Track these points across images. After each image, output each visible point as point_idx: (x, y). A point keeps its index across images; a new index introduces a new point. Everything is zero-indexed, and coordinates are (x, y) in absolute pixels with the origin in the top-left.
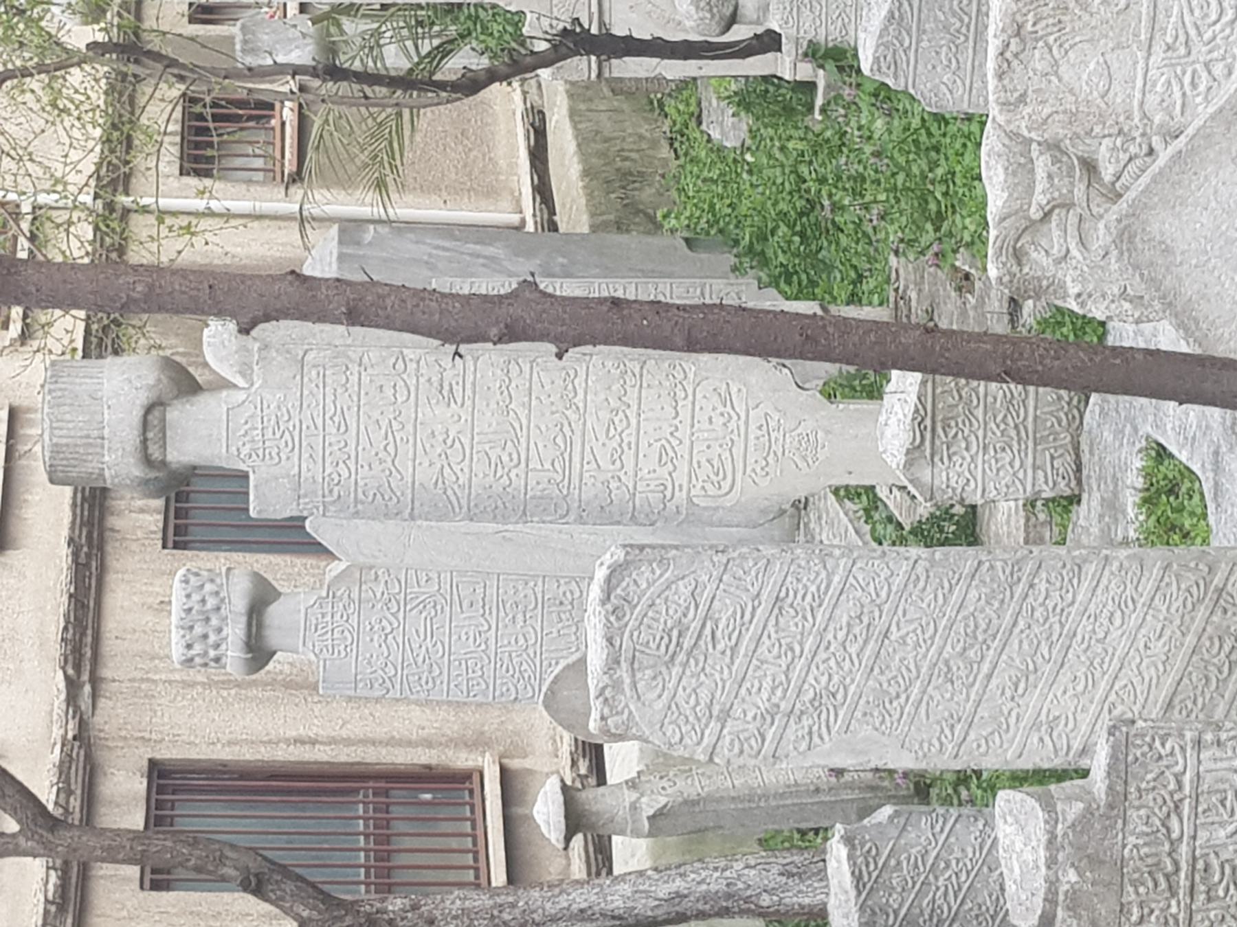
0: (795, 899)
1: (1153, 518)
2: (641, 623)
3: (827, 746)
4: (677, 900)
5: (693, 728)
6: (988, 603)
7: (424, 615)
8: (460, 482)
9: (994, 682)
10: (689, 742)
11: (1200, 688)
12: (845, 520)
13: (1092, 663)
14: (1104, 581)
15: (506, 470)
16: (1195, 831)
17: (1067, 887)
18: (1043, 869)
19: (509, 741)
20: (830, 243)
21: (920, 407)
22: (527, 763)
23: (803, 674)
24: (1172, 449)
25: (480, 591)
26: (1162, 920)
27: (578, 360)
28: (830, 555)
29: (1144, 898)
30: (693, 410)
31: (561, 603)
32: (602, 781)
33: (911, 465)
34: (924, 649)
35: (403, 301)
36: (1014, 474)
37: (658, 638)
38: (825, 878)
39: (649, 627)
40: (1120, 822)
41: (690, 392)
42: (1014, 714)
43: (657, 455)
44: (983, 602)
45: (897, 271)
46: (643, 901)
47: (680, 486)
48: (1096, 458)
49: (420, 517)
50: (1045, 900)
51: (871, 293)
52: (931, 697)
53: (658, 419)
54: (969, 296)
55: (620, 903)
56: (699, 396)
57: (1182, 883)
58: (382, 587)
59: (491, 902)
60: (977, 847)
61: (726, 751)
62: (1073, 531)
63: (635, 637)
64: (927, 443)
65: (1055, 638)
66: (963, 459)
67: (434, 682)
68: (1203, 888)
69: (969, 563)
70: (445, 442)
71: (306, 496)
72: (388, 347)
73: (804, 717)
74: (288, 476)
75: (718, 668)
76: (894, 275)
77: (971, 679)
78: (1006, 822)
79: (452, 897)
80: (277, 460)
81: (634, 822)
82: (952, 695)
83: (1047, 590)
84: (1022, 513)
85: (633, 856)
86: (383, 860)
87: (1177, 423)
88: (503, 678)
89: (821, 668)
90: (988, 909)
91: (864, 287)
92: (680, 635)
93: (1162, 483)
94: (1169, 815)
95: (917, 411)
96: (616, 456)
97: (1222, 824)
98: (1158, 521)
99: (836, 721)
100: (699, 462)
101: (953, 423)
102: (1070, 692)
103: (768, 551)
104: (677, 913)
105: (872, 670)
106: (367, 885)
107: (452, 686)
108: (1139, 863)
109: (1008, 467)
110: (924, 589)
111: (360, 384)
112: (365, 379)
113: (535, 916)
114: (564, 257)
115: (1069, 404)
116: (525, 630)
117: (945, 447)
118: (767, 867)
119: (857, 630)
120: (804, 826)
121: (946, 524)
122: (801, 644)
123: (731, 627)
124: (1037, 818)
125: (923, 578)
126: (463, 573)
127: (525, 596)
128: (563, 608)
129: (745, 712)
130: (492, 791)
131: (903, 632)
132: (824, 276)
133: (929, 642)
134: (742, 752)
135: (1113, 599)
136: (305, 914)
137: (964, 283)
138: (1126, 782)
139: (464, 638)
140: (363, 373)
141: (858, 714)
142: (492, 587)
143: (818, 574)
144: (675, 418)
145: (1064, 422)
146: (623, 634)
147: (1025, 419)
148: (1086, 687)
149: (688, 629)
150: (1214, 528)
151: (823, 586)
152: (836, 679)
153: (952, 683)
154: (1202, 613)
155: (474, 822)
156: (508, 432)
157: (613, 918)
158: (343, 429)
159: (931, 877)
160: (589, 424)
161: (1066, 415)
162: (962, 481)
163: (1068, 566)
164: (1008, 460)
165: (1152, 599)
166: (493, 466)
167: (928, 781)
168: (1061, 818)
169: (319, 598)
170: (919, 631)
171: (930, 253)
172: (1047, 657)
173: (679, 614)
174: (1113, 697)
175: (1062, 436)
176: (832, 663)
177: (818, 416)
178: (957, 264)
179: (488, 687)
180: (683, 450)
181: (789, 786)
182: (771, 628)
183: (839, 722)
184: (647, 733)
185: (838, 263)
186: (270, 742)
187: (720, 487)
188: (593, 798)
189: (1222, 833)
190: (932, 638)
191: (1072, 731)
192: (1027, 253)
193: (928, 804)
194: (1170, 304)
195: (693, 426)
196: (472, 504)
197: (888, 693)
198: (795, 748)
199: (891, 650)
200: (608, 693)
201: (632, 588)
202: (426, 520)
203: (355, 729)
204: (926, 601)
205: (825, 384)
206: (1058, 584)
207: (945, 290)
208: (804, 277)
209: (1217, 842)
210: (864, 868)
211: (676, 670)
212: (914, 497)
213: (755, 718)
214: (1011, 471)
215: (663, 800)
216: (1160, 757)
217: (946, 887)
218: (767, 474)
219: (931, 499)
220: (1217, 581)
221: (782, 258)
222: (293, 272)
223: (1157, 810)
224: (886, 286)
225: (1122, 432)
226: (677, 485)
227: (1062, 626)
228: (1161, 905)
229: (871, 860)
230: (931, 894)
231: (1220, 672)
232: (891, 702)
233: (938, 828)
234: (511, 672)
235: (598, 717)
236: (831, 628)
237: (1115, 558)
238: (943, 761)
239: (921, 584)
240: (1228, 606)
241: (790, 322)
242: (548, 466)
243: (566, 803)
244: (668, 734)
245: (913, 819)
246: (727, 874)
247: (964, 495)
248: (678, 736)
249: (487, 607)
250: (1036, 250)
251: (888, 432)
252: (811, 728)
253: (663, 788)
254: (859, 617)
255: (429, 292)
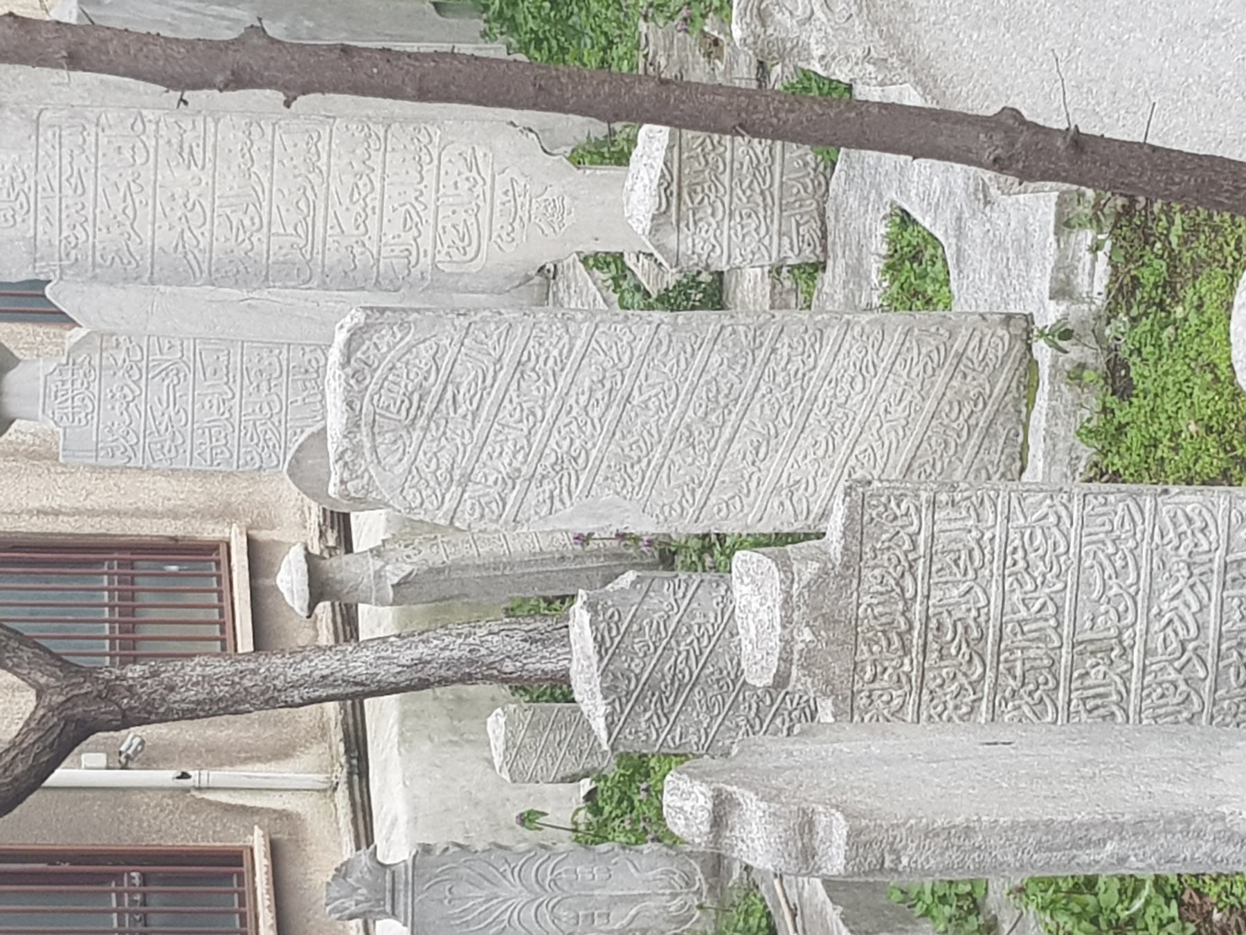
0: (538, 665)
1: (897, 284)
2: (381, 387)
3: (568, 510)
4: (420, 667)
5: (434, 493)
6: (729, 367)
7: (166, 382)
8: (201, 246)
9: (736, 446)
10: (431, 507)
11: (939, 453)
12: (594, 289)
13: (832, 428)
14: (846, 346)
15: (248, 234)
16: (929, 590)
17: (803, 645)
18: (779, 629)
19: (256, 512)
20: (581, 9)
21: (666, 172)
22: (274, 535)
23: (545, 439)
24: (916, 215)
25: (223, 358)
26: (895, 678)
27: (321, 122)
28: (572, 319)
29: (878, 656)
30: (439, 174)
31: (307, 371)
32: (349, 550)
33: (657, 231)
34: (666, 414)
35: (126, 45)
36: (760, 241)
37: (398, 403)
38: (568, 644)
39: (390, 390)
40: (855, 582)
41: (435, 156)
42: (755, 478)
43: (402, 220)
44: (725, 366)
45: (646, 36)
46: (386, 667)
47: (425, 251)
48: (842, 224)
49: (160, 281)
50: (779, 659)
51: (620, 59)
52: (673, 462)
53: (402, 183)
54: (717, 61)
55: (362, 670)
56: (444, 159)
57: (915, 642)
58: (123, 355)
59: (232, 669)
60: (719, 613)
61: (467, 516)
62: (818, 298)
63: (375, 402)
64: (673, 209)
65: (796, 402)
66: (710, 225)
67: (177, 451)
68: (935, 646)
69: (712, 327)
70: (185, 205)
71: (42, 258)
72: (126, 108)
73: (545, 482)
74: (24, 238)
75: (459, 432)
76: (643, 41)
77: (712, 444)
78: (742, 582)
79: (192, 664)
80: (12, 222)
81: (378, 591)
82: (694, 460)
83: (789, 354)
84: (768, 281)
85: (379, 625)
86: (127, 632)
87: (921, 189)
88: (247, 446)
89: (563, 433)
90: (729, 673)
91: (614, 54)
92: (421, 399)
93: (906, 249)
94: (903, 575)
95: (663, 176)
96: (360, 221)
97: (956, 584)
98: (902, 288)
99: (577, 485)
100: (444, 228)
101: (699, 189)
102: (811, 457)
103: (510, 315)
104: (420, 679)
105: (614, 434)
106: (112, 656)
107: (195, 454)
108: (873, 622)
109: (754, 234)
110: (666, 353)
111: (97, 145)
112: (103, 140)
113: (276, 682)
114: (309, 19)
115: (815, 170)
116: (269, 398)
117: (691, 212)
118: (510, 633)
119: (599, 395)
120: (550, 593)
121: (693, 291)
122: (543, 408)
123: (472, 392)
124: (773, 578)
125: (665, 343)
126: (205, 340)
127: (270, 364)
128: (307, 376)
129: (485, 476)
130: (238, 562)
131: (645, 397)
132: (574, 42)
133: (671, 407)
134: (482, 516)
135: (855, 365)
136: (43, 680)
137: (713, 49)
138: (861, 543)
139: (207, 406)
140: (101, 134)
141: (599, 479)
142: (235, 354)
143: (560, 339)
144: (420, 182)
145: (810, 189)
146: (363, 397)
147: (771, 186)
148: (826, 451)
149: (429, 393)
150: (956, 293)
151: (565, 351)
152: (577, 443)
153: (694, 448)
154: (941, 377)
155: (220, 593)
156: (250, 195)
157: (356, 684)
158: (80, 191)
159: (673, 641)
160: (332, 188)
161: (812, 181)
162: (708, 248)
163: (810, 332)
164: (754, 226)
165: (894, 363)
166: (234, 230)
167: (673, 549)
168: (797, 578)
169: (59, 365)
170: (661, 396)
171: (679, 18)
172: (788, 422)
173: (420, 377)
174: (852, 462)
175: (808, 202)
176: (574, 427)
177: (564, 182)
178: (706, 29)
179: (231, 456)
180: (428, 215)
181: (535, 554)
182: (512, 392)
183: (580, 486)
184: (388, 497)
185: (588, 30)
186: (12, 513)
187: (465, 254)
188: (342, 568)
189: (955, 592)
190: (674, 402)
191: (812, 496)
192: (771, 14)
193: (673, 570)
194: (909, 61)
195: (437, 191)
196: (213, 269)
197: (630, 457)
198: (536, 513)
199: (633, 414)
200: (347, 457)
201: (373, 351)
202: (166, 284)
203: (99, 500)
204: (669, 365)
205: (573, 151)
206: (800, 349)
207: (693, 56)
208: (554, 43)
209: (952, 601)
210: (606, 634)
211: (417, 434)
212: (660, 264)
213: (496, 483)
214: (757, 238)
215: (408, 569)
216: (896, 518)
217: (688, 651)
218: (513, 240)
219: (677, 265)
220: (958, 345)
221: (531, 24)
222: (11, 14)
223: (891, 570)
224: (635, 52)
225: (867, 198)
226: (421, 250)
227: (804, 391)
228: (894, 663)
229: (613, 625)
230: (673, 659)
231: (959, 436)
232: (632, 467)
233: (680, 594)
234: (256, 441)
235: (338, 481)
236: (572, 392)
237: (858, 322)
238: (683, 526)
239: (664, 349)
240: (967, 371)
241: (523, 71)
242: (290, 230)
243: (309, 571)
244: (409, 498)
245: (656, 584)
246: (470, 640)
247: (710, 261)
248: (418, 501)
249: (231, 375)
250: (780, 10)
251: (634, 198)
252: (552, 492)
253: (408, 557)
254: (601, 382)
255: (153, 36)
